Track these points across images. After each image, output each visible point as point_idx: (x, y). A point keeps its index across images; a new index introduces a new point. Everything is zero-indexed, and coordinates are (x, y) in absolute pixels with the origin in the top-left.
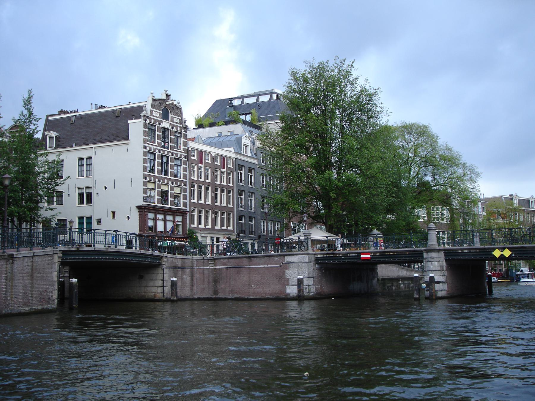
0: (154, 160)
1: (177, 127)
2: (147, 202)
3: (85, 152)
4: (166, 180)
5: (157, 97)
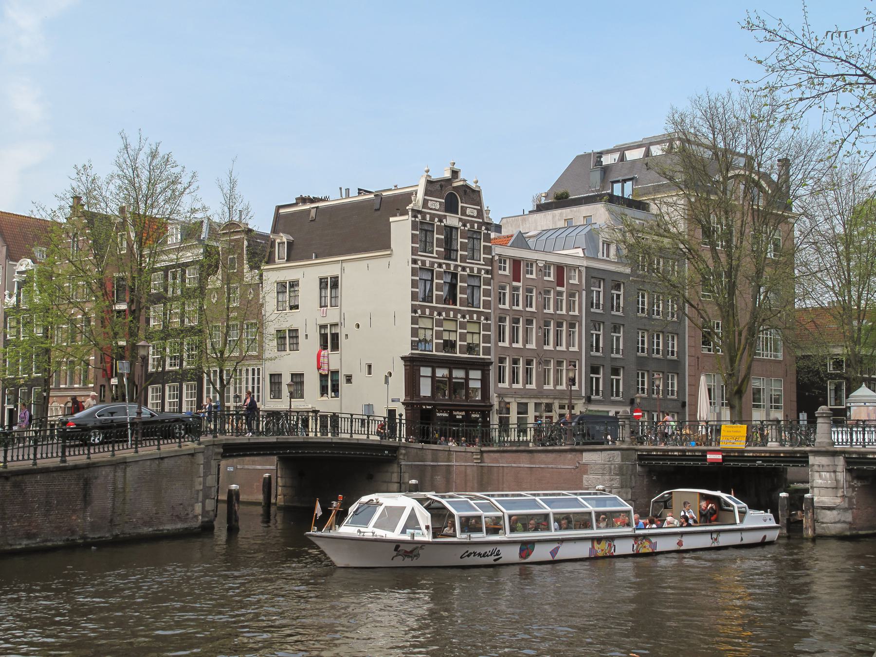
0: (432, 280)
1: (472, 223)
2: (417, 350)
3: (329, 268)
4: (452, 313)
5: (435, 177)
